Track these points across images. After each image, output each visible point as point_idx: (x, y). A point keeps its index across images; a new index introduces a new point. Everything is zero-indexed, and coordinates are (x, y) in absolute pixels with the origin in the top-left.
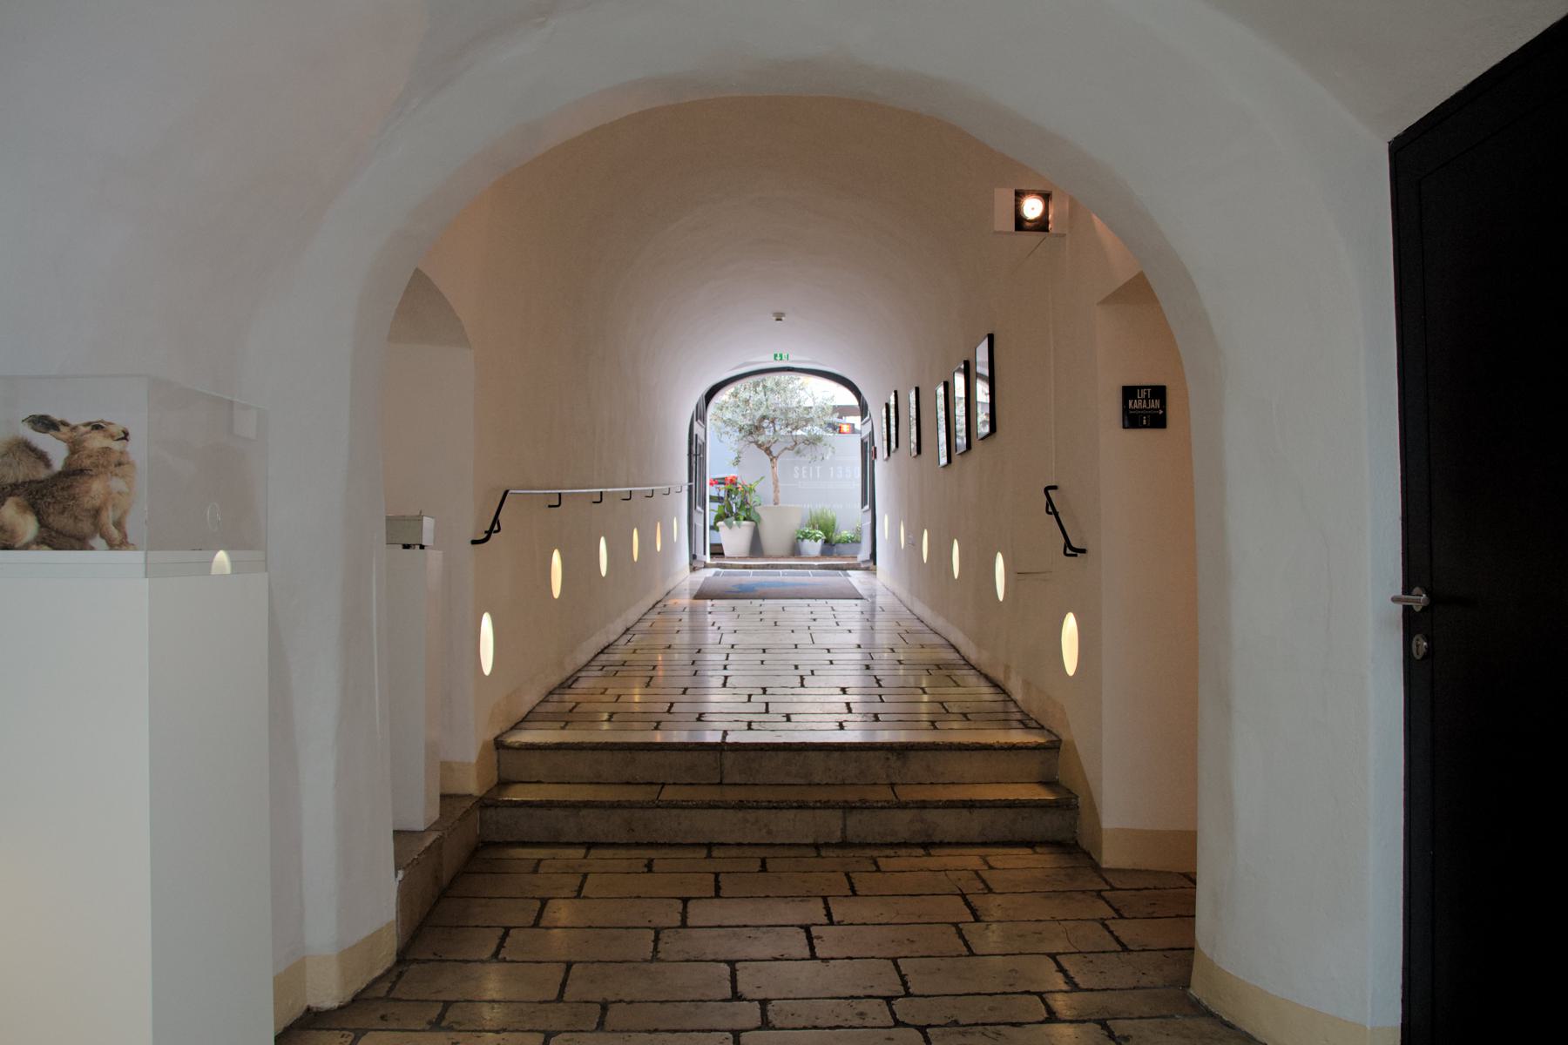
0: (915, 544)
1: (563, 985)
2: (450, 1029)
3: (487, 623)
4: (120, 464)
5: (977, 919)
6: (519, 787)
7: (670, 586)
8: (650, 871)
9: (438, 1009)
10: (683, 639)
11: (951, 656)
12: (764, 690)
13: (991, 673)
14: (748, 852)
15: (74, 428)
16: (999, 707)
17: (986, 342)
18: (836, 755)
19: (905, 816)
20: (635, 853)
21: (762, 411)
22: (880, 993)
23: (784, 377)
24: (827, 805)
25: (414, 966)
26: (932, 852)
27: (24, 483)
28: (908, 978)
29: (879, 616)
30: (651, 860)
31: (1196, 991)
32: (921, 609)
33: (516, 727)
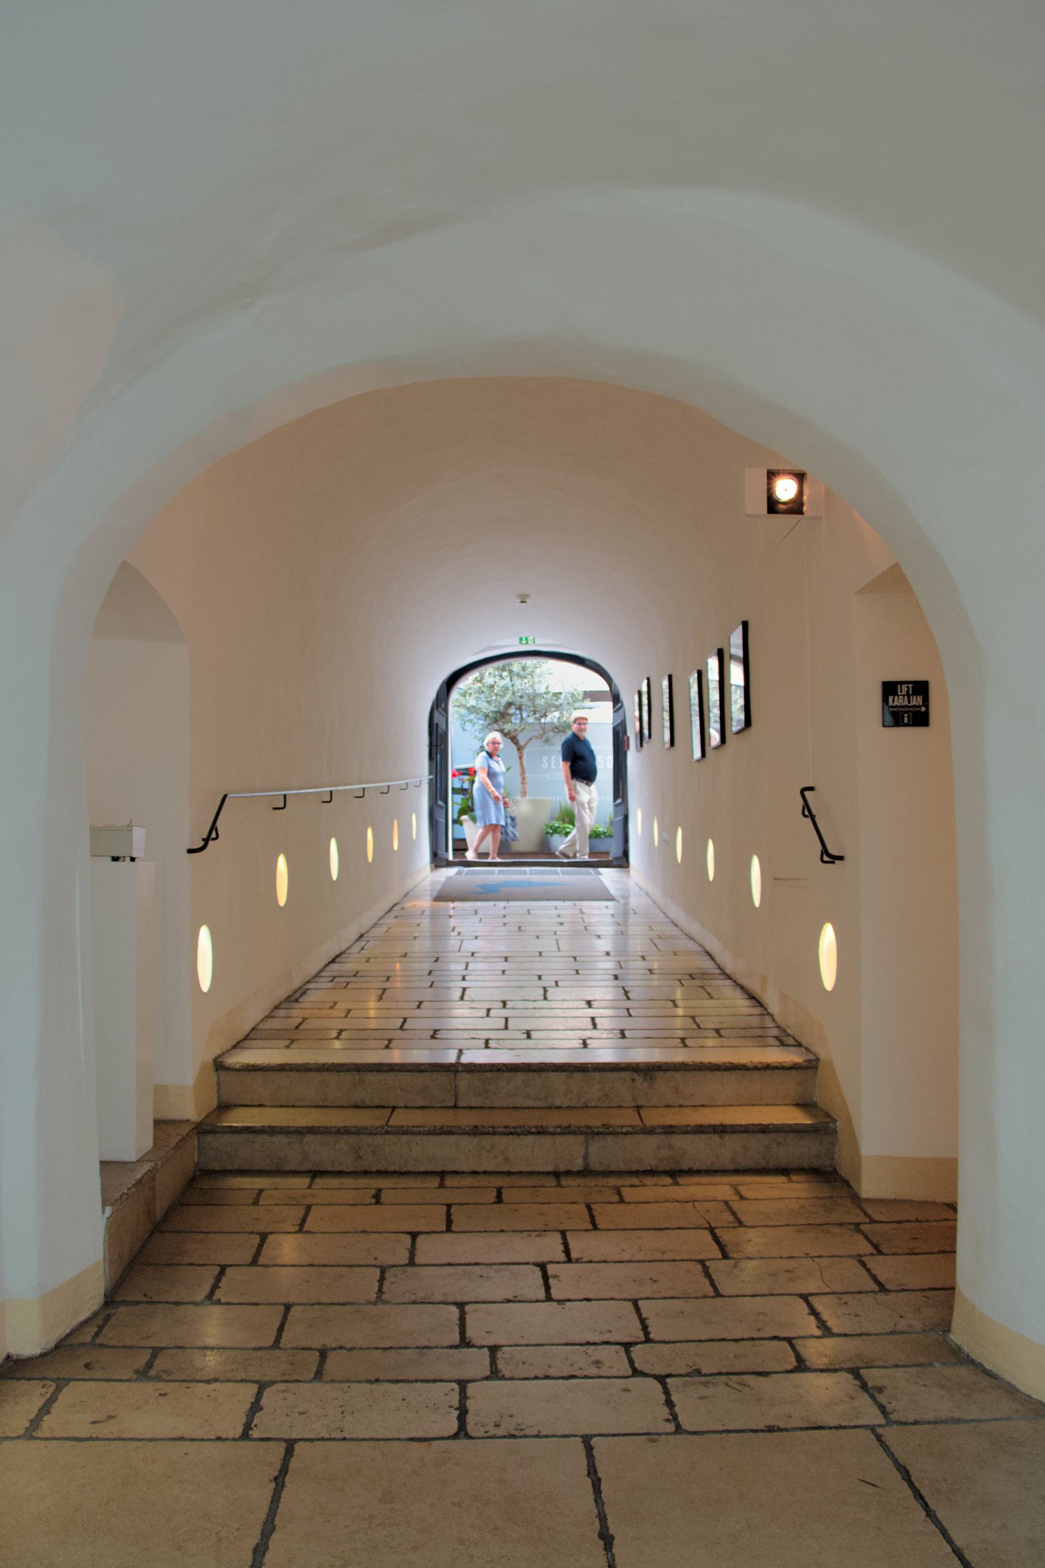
0: (668, 843)
1: (281, 1330)
2: (158, 1378)
3: (205, 937)
5: (725, 1256)
6: (241, 1111)
7: (408, 886)
8: (378, 1202)
9: (144, 1358)
10: (423, 946)
11: (708, 964)
12: (504, 1003)
13: (745, 982)
14: (483, 1181)
16: (755, 1021)
17: (740, 629)
18: (578, 1076)
19: (654, 1140)
20: (363, 1182)
21: (508, 698)
22: (619, 1339)
23: (529, 662)
24: (568, 1131)
25: (122, 1309)
26: (681, 1180)
28: (648, 1322)
29: (633, 919)
30: (379, 1190)
31: (957, 1336)
32: (676, 913)
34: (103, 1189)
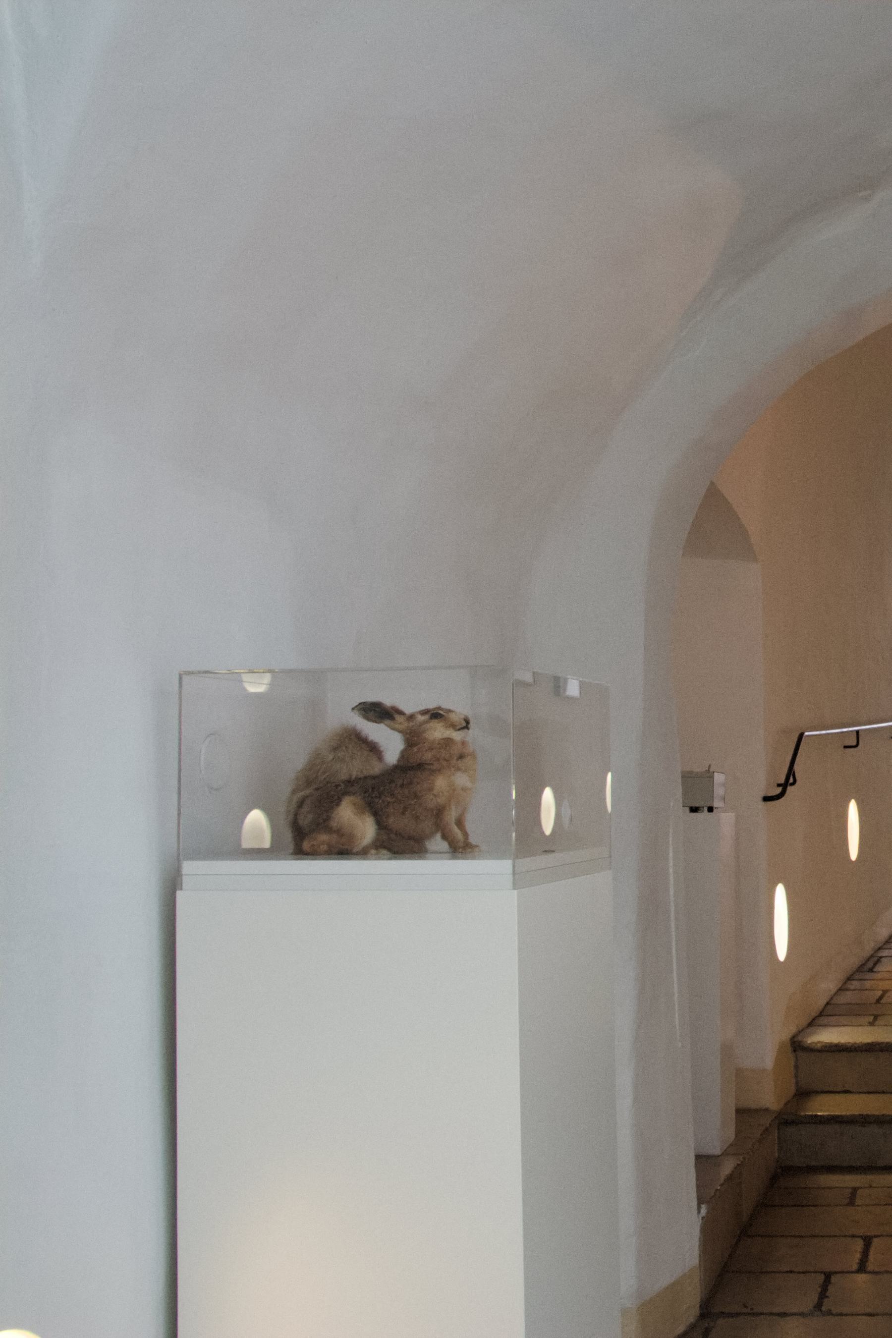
4: (461, 757)
15: (411, 717)
25: (721, 1321)
27: (358, 780)
33: (813, 1023)
34: (698, 1186)
